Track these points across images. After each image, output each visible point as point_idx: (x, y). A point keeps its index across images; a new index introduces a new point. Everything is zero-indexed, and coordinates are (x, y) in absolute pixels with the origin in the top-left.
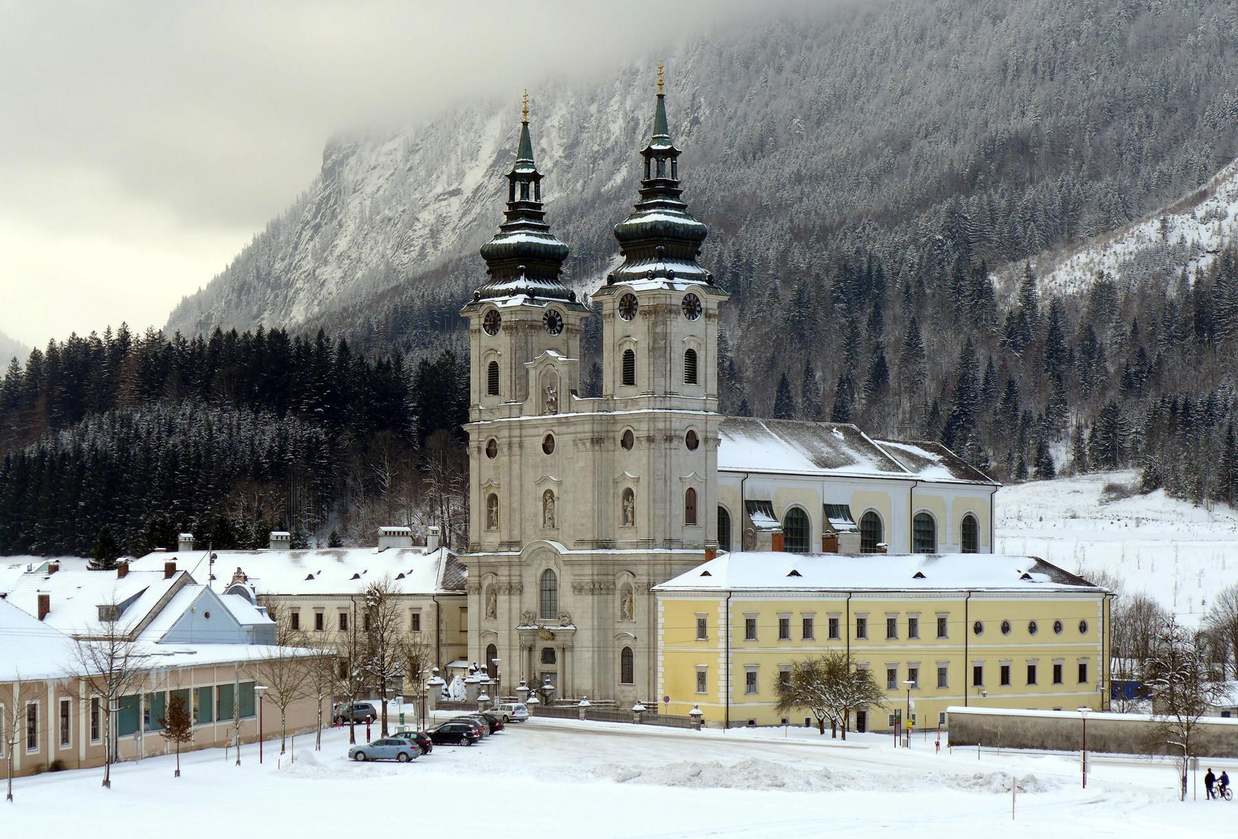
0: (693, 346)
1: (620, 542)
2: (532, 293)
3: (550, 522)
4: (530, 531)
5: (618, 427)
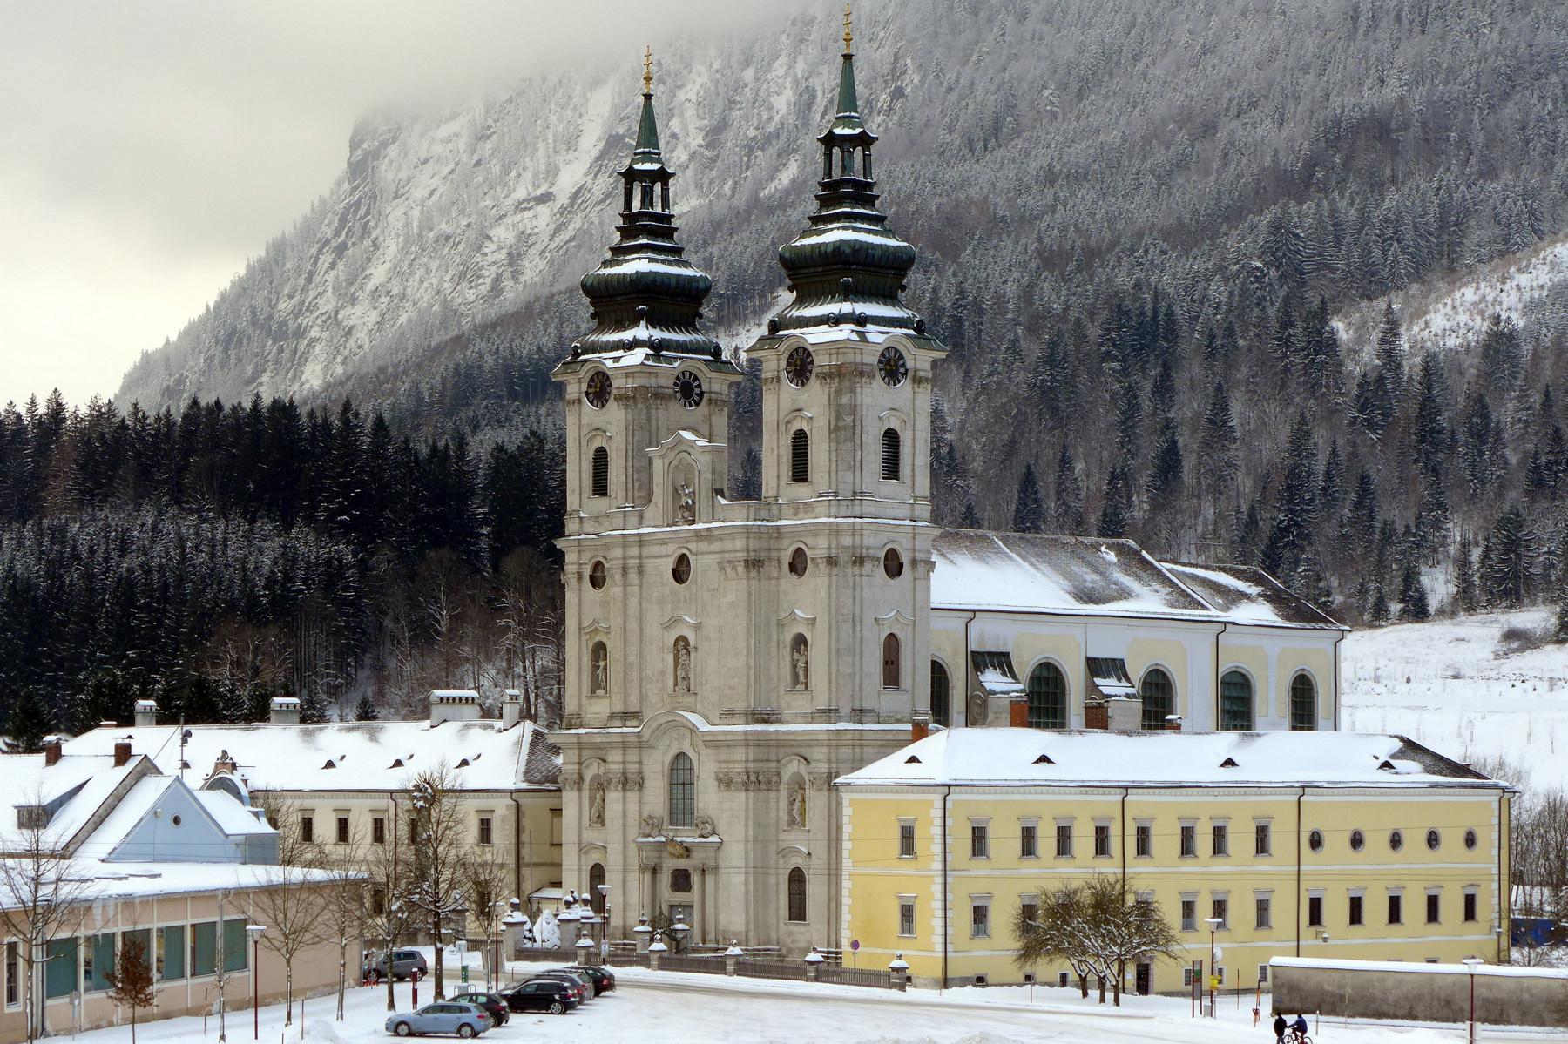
0: (894, 424)
2: (657, 347)
3: (684, 682)
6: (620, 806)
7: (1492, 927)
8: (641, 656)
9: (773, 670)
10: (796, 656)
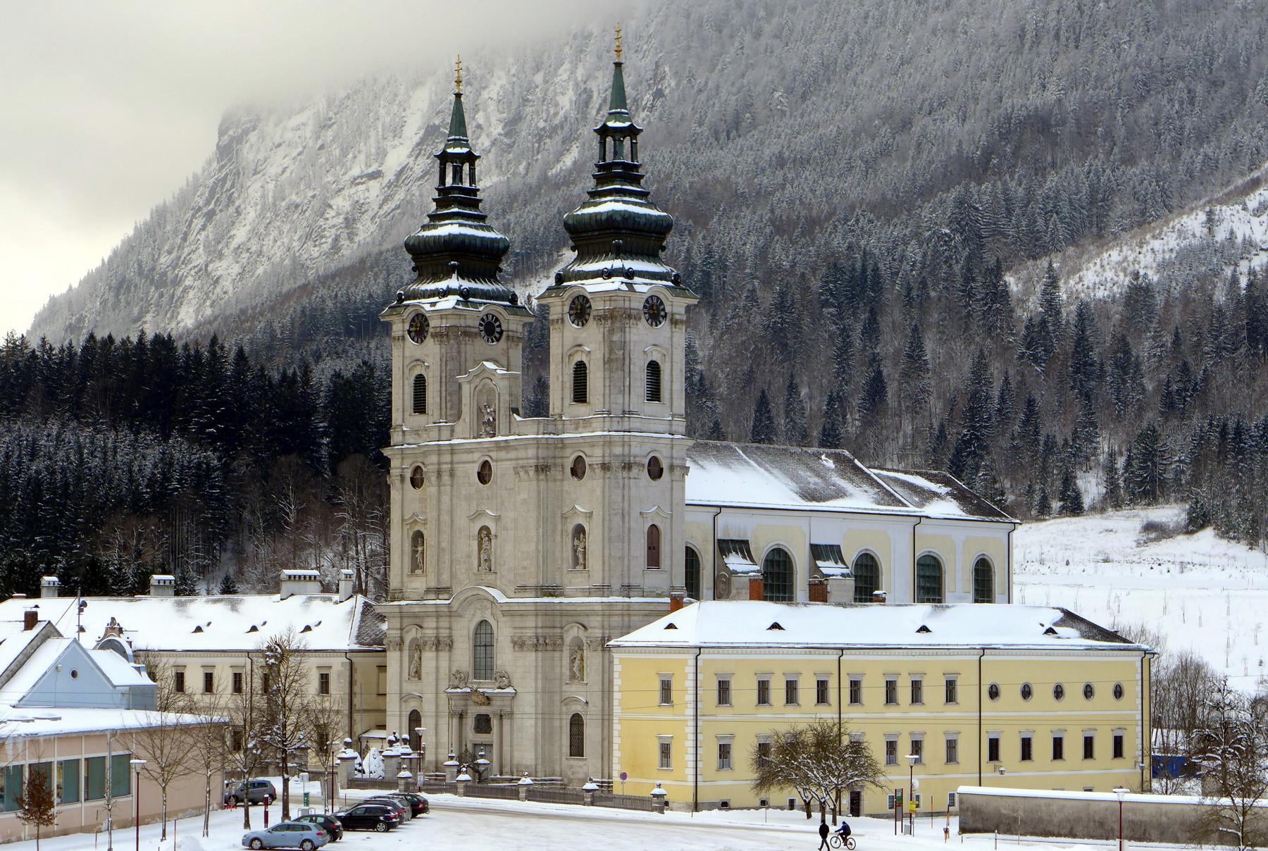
0: (656, 357)
2: (465, 295)
3: (486, 564)
5: (568, 452)
6: (434, 663)
7: (1136, 762)
8: (452, 543)
9: (558, 554)
10: (576, 542)
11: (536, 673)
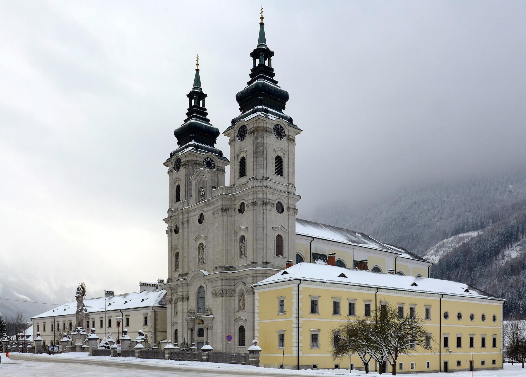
0: (280, 154)
1: (237, 266)
2: (197, 147)
3: (202, 260)
4: (192, 268)
5: (237, 202)
7: (501, 349)
8: (188, 253)
10: (241, 244)
11: (222, 307)
